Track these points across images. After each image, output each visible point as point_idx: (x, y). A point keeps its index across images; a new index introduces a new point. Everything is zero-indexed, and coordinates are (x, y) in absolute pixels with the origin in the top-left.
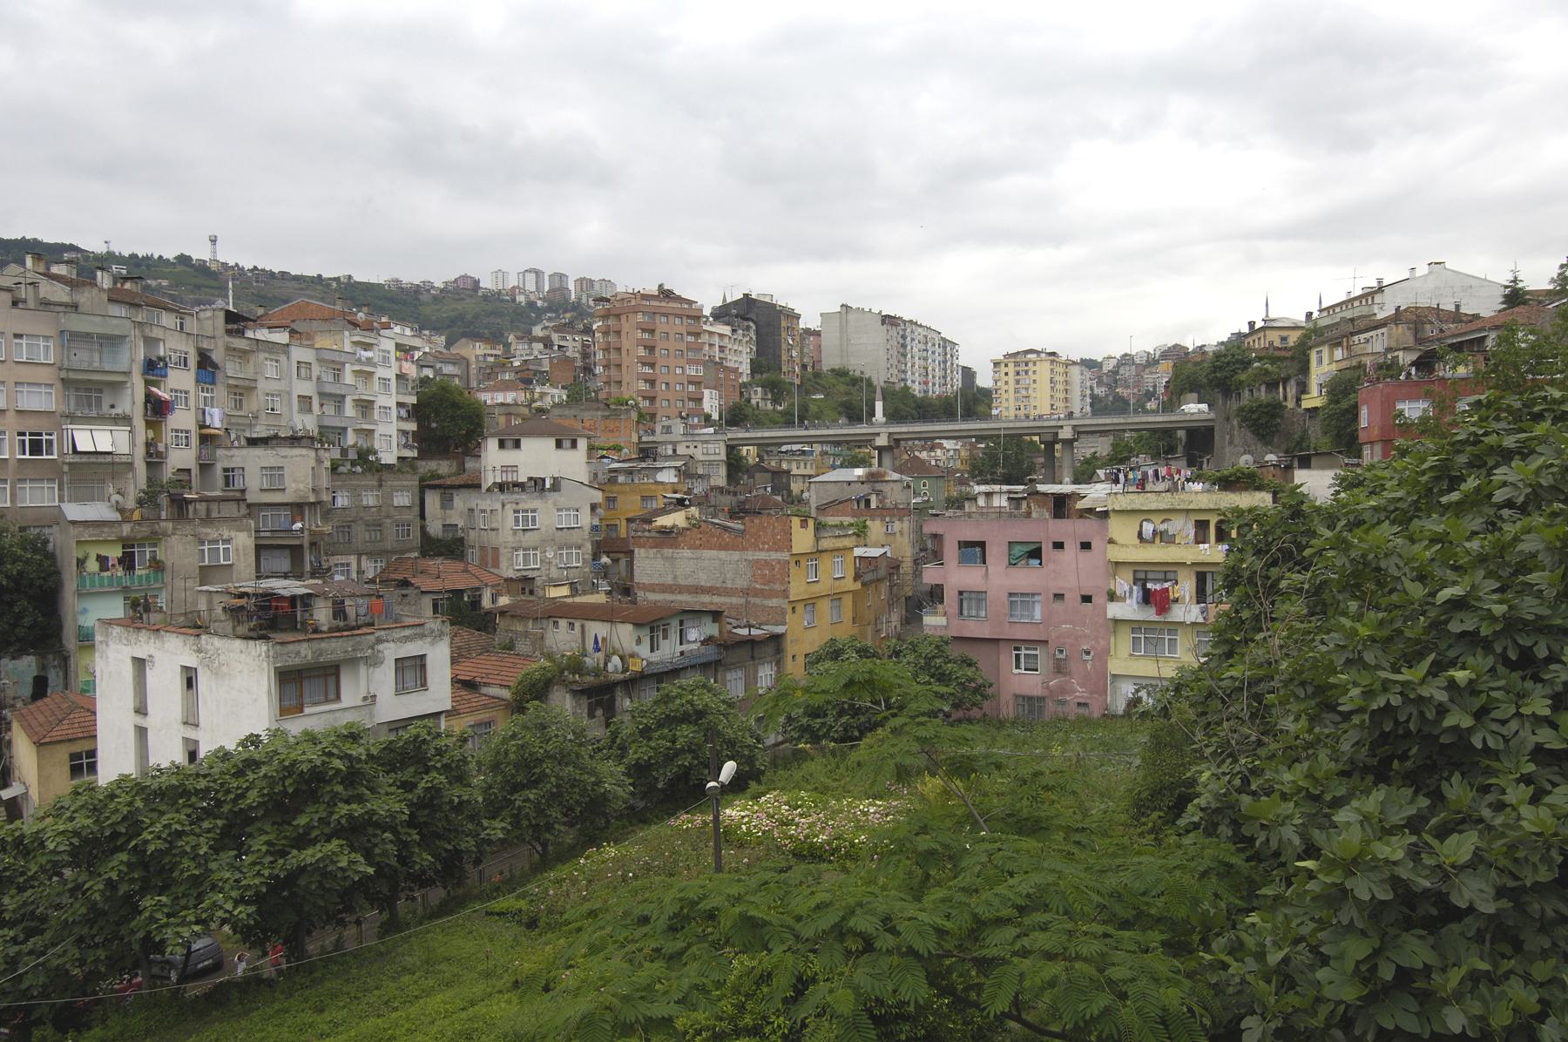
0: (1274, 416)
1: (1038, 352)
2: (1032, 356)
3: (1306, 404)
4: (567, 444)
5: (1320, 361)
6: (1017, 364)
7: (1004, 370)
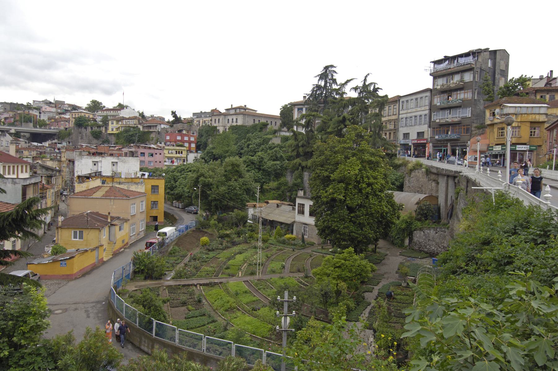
5: (113, 124)
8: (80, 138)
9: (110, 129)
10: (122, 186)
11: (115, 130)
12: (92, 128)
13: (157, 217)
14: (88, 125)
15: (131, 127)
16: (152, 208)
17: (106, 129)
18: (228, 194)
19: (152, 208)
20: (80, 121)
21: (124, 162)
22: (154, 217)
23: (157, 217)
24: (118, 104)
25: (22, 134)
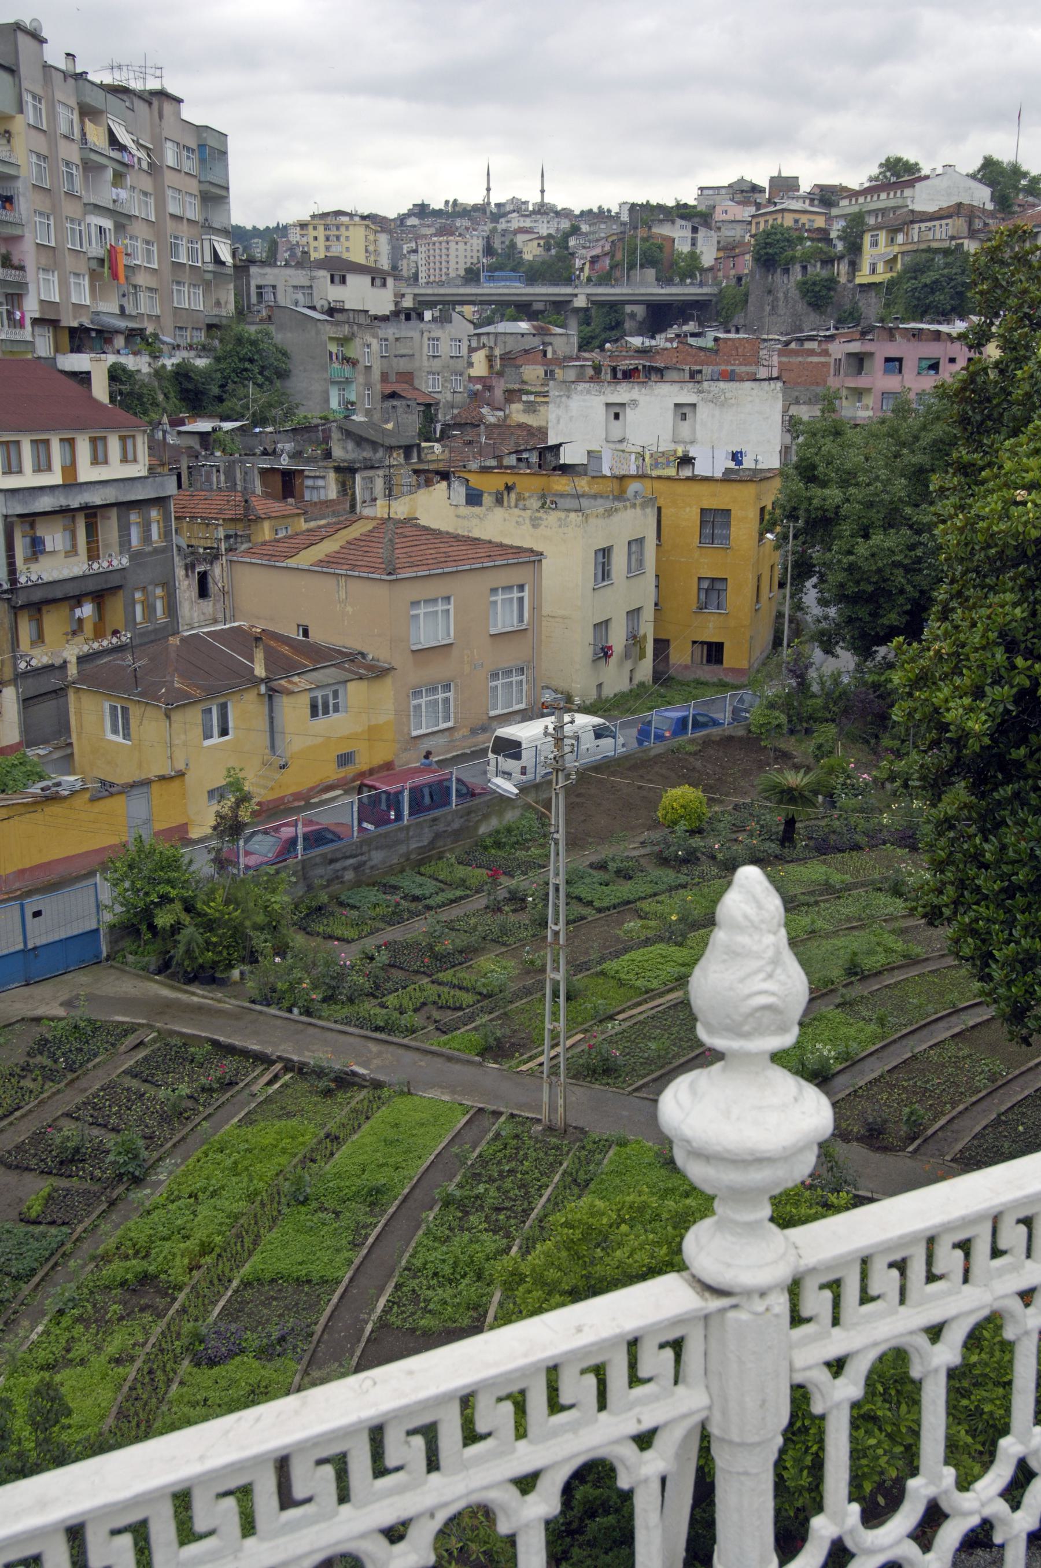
0: (829, 289)
1: (351, 215)
2: (345, 219)
3: (858, 280)
4: (378, 282)
5: (875, 244)
6: (327, 227)
7: (312, 233)
8: (768, 308)
9: (866, 268)
10: (323, 522)
11: (880, 267)
12: (804, 268)
13: (719, 646)
14: (792, 259)
15: (936, 251)
16: (702, 607)
17: (854, 266)
18: (907, 570)
19: (702, 607)
20: (770, 245)
21: (722, 405)
22: (710, 644)
23: (719, 646)
24: (978, 163)
25: (628, 309)
